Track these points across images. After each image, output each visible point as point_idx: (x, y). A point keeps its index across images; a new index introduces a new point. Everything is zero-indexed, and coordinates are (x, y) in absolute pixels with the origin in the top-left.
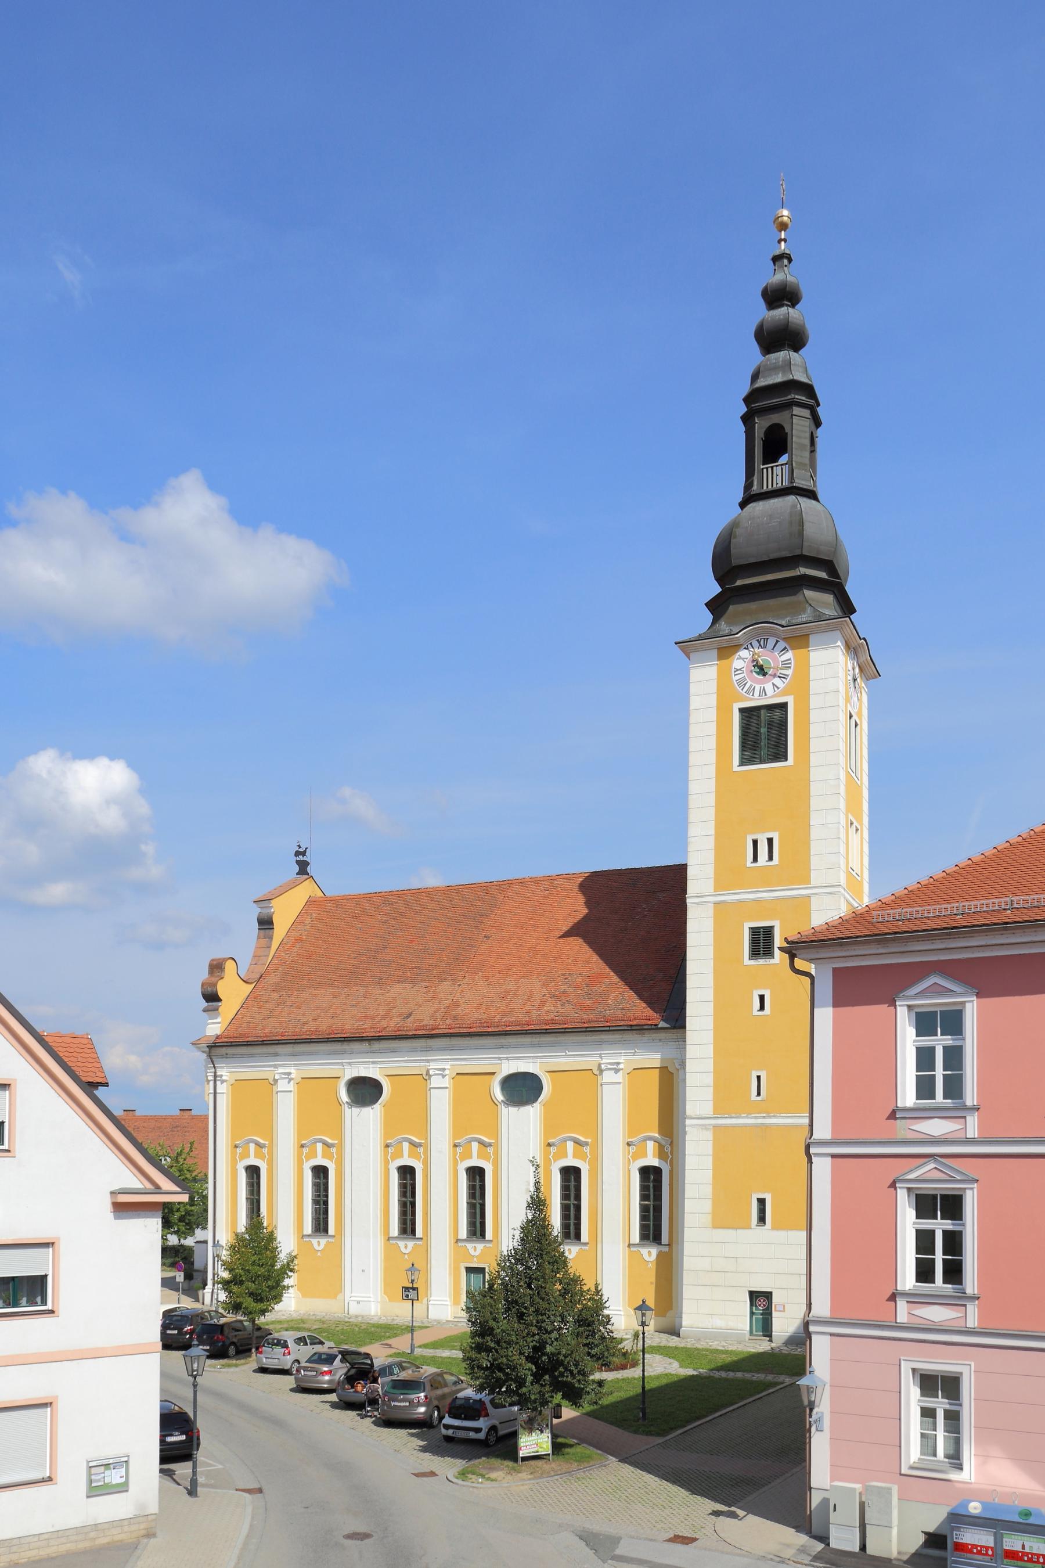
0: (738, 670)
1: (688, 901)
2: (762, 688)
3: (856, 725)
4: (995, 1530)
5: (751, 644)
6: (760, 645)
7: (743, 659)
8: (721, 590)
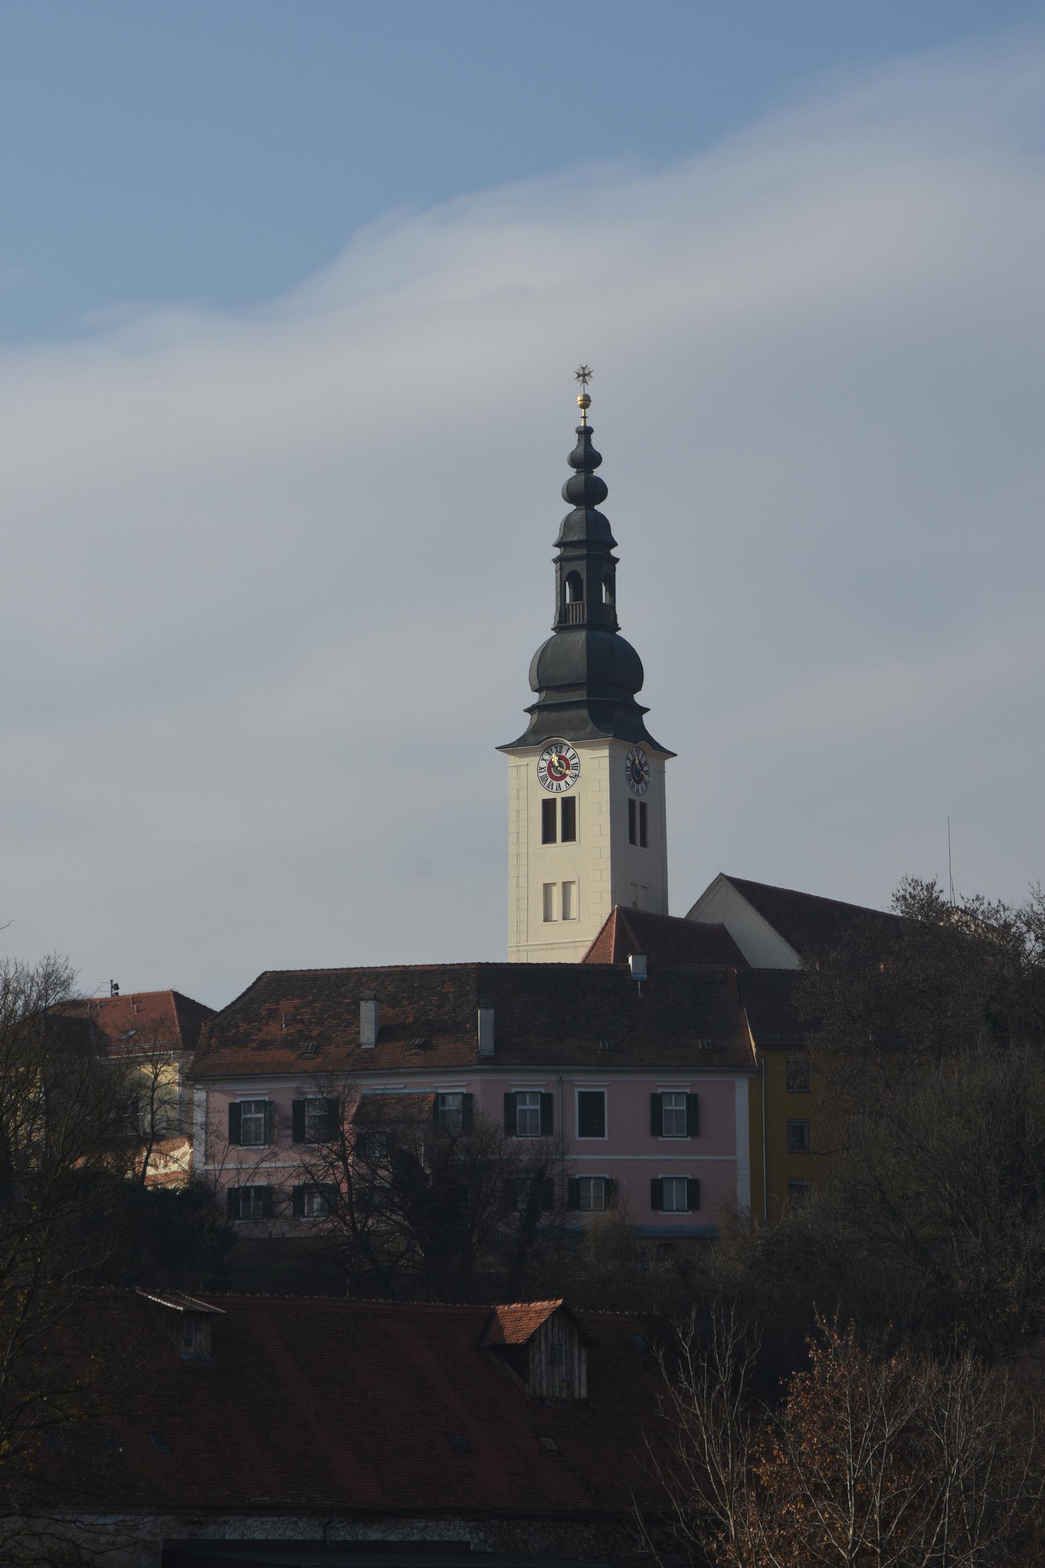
0: (542, 768)
6: (557, 751)
7: (545, 760)
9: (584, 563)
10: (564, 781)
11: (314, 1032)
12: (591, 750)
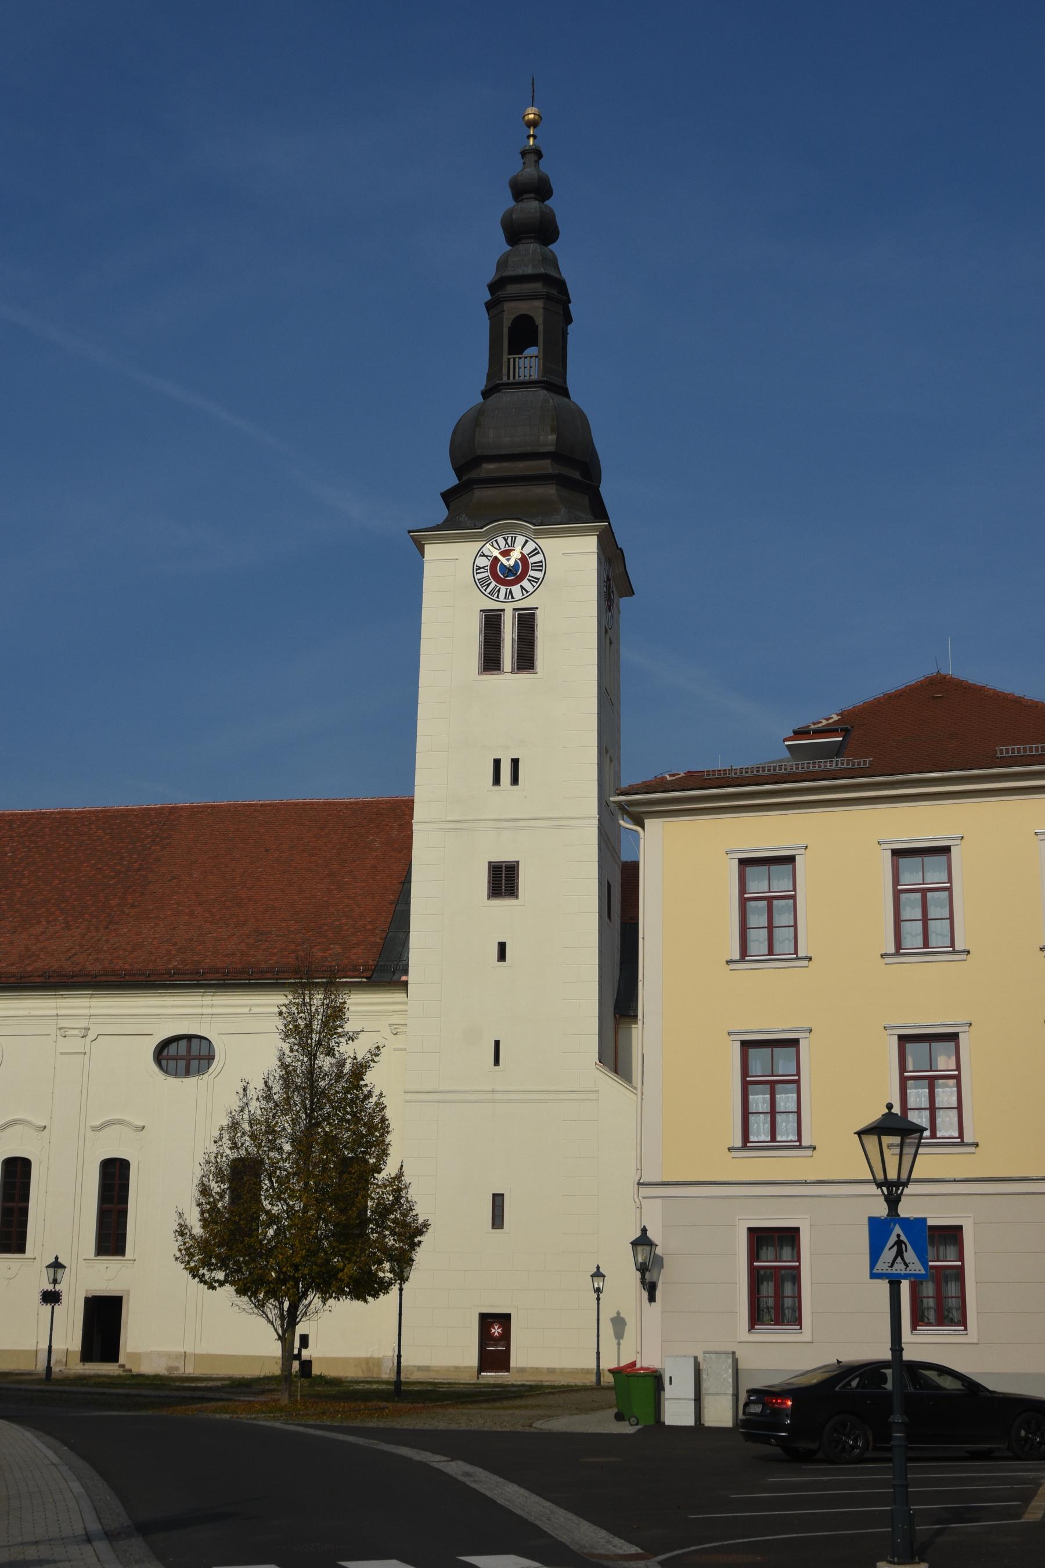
0: (480, 568)
1: (414, 827)
2: (508, 590)
3: (611, 643)
5: (496, 541)
6: (507, 543)
7: (487, 556)
8: (457, 482)
9: (539, 304)
10: (519, 585)
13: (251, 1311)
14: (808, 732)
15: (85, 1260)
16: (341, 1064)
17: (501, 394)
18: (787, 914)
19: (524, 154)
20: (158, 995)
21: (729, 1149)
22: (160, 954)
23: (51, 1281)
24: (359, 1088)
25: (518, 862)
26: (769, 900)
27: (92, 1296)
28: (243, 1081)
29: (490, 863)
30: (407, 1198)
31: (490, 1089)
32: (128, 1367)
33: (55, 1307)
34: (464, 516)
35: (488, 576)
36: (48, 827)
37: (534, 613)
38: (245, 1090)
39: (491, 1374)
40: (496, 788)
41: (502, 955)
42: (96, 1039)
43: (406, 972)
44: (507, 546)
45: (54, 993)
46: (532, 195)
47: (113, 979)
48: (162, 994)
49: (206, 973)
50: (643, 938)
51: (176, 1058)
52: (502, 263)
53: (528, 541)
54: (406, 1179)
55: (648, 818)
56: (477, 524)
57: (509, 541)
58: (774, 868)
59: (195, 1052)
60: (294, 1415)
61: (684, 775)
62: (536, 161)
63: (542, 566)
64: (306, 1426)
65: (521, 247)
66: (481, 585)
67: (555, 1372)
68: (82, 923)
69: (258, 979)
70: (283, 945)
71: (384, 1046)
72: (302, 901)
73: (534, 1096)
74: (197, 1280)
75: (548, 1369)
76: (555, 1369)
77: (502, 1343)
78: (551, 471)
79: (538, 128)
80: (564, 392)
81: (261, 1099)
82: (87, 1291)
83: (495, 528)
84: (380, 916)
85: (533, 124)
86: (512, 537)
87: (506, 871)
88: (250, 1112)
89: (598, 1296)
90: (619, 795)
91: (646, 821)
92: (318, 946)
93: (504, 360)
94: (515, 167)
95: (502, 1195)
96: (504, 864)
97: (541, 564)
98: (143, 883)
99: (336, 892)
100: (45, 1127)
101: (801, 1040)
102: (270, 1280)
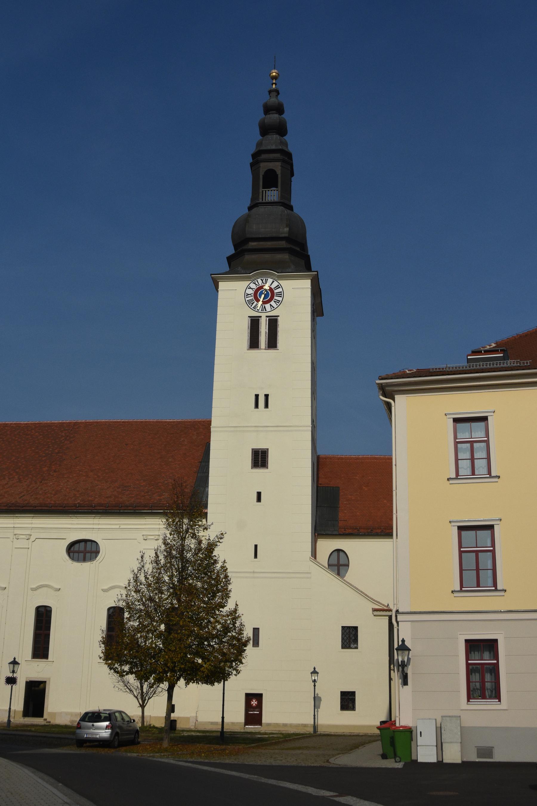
0: (248, 295)
1: (212, 429)
2: (263, 306)
4: (457, 440)
5: (257, 281)
6: (263, 282)
7: (252, 289)
11: (193, 541)
12: (247, 213)
13: (125, 690)
14: (481, 352)
15: (26, 661)
16: (200, 542)
17: (259, 208)
18: (481, 452)
19: (270, 92)
20: (70, 517)
21: (452, 592)
22: (70, 496)
23: (11, 672)
24: (211, 557)
25: (268, 449)
26: (472, 443)
27: (30, 681)
28: (141, 552)
29: (253, 449)
30: (242, 623)
31: (252, 571)
32: (48, 720)
33: (13, 686)
34: (240, 268)
35: (253, 299)
36: (9, 431)
37: (277, 319)
38: (142, 557)
39: (251, 726)
40: (257, 409)
41: (259, 499)
42: (34, 541)
43: (206, 507)
44: (263, 284)
45: (13, 516)
46: (274, 112)
47: (46, 508)
48: (72, 517)
49: (96, 506)
50: (396, 465)
51: (79, 552)
52: (259, 144)
53: (274, 281)
54: (239, 612)
55: (397, 395)
56: (247, 272)
57: (264, 281)
58: (474, 424)
59: (88, 549)
60: (176, 754)
61: (416, 371)
62: (276, 96)
63: (281, 294)
64: (186, 762)
65: (269, 137)
66: (249, 303)
67: (287, 725)
68: (27, 479)
69: (124, 510)
70: (137, 493)
71: (226, 533)
72: (147, 470)
73: (275, 575)
74: (112, 671)
75: (283, 724)
76: (287, 724)
77: (257, 710)
78: (285, 247)
79: (277, 80)
80: (291, 208)
81: (153, 562)
82: (27, 678)
83: (254, 275)
84: (189, 479)
85: (275, 78)
86: (266, 279)
87: (261, 454)
88: (145, 571)
89: (315, 684)
90: (380, 379)
91: (396, 396)
92: (156, 493)
93: (260, 191)
94: (265, 98)
95: (258, 629)
96: (260, 450)
97: (281, 293)
98: (61, 460)
99: (165, 466)
100: (5, 588)
101: (495, 525)
102: (161, 671)
